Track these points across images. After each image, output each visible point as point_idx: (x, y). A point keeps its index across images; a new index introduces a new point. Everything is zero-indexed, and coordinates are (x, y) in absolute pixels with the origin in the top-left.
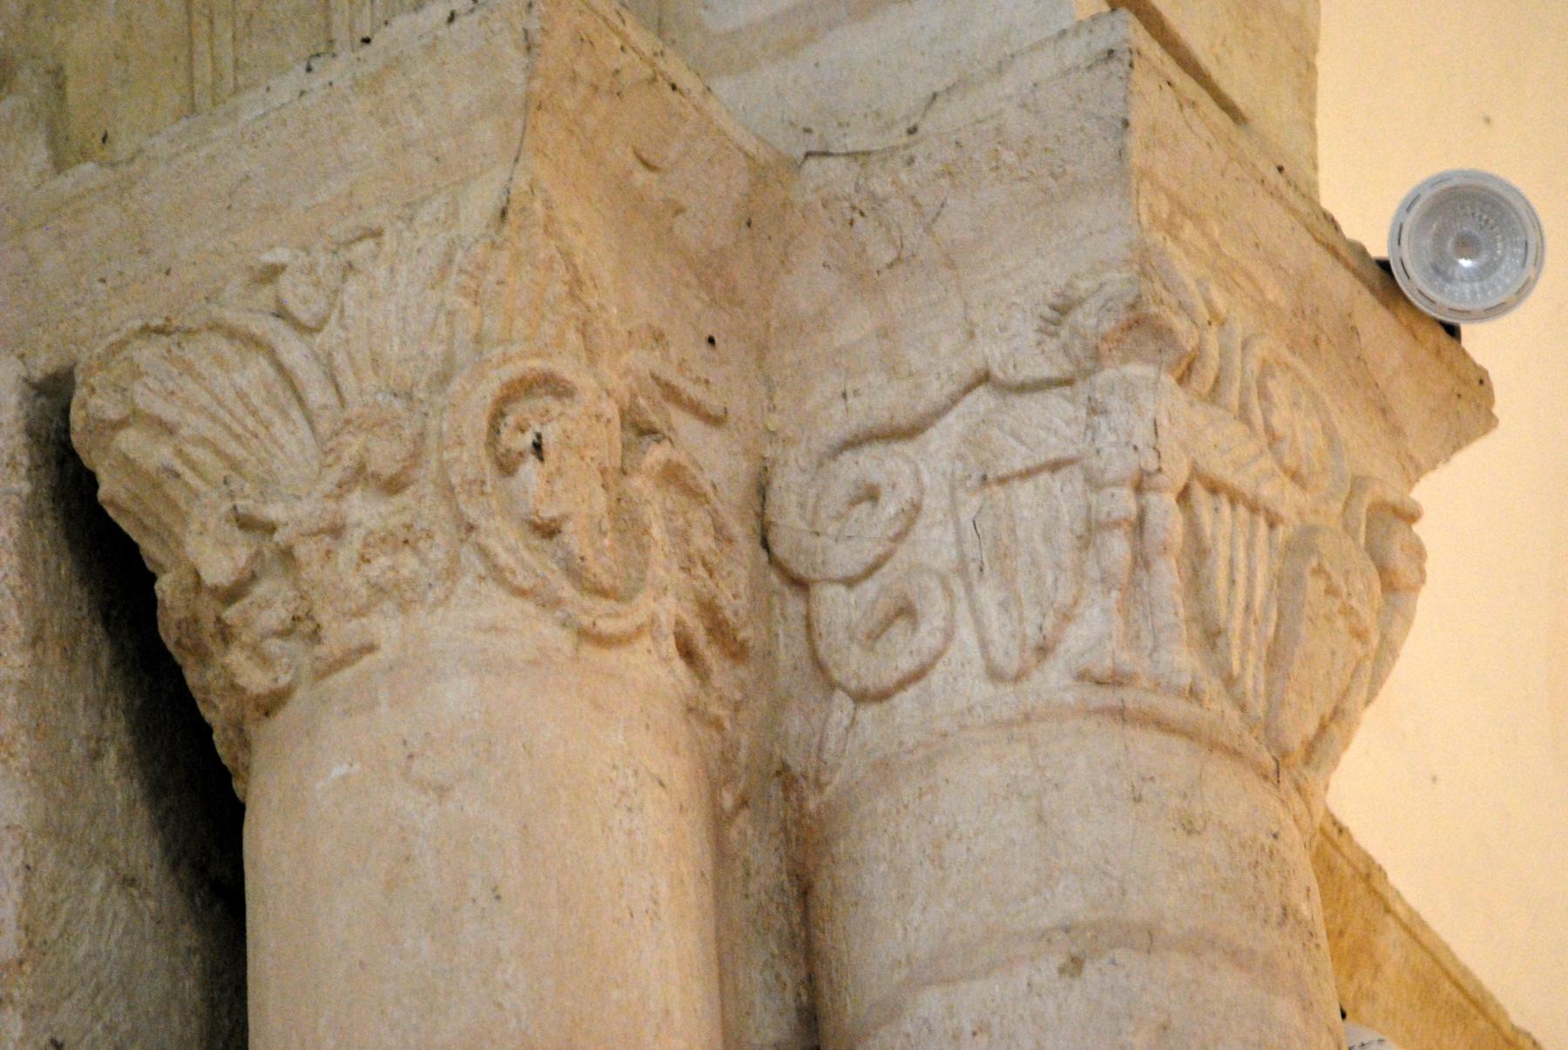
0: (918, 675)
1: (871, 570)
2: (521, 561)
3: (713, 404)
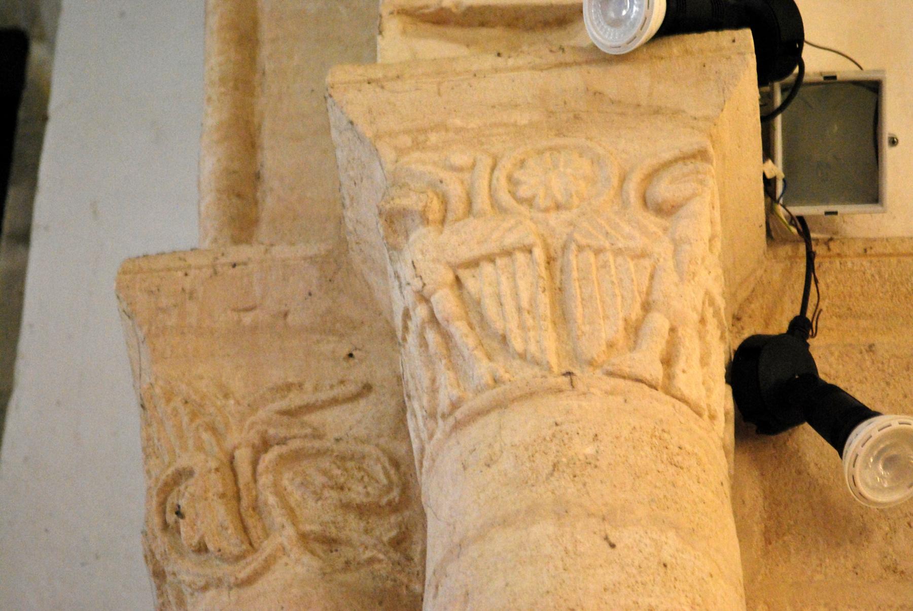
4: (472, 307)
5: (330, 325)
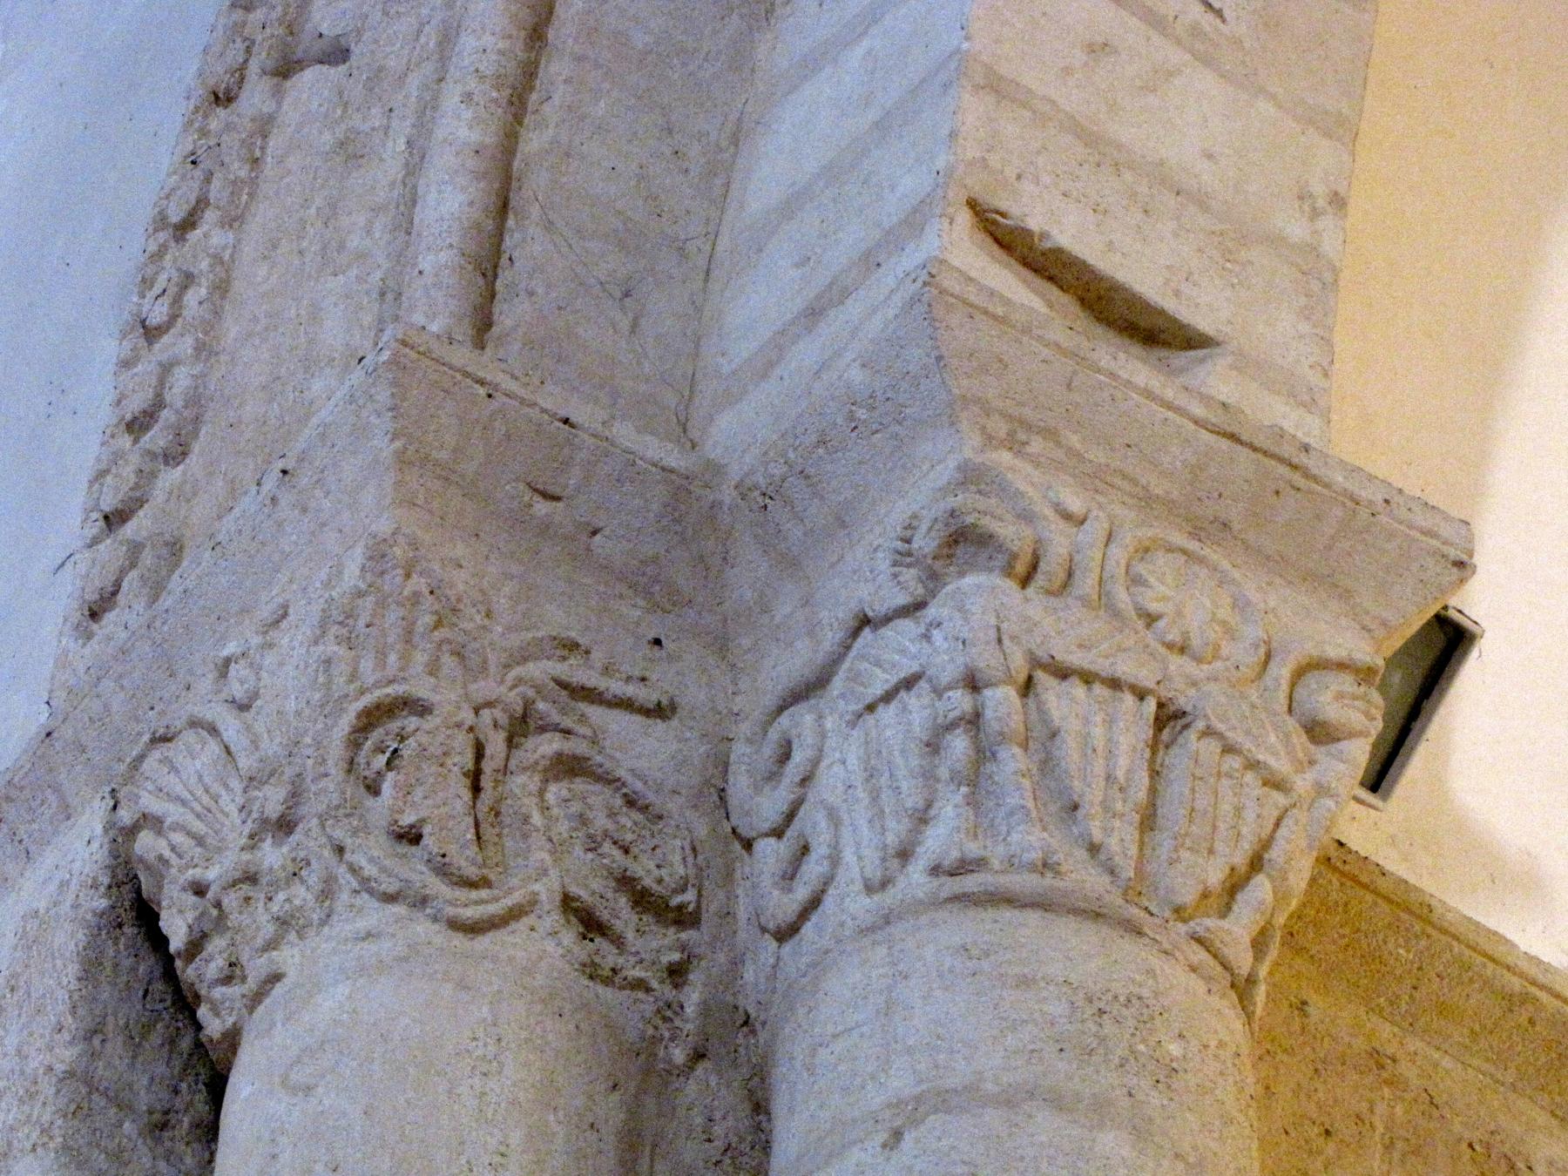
2: (383, 870)
4: (1043, 740)
5: (646, 583)
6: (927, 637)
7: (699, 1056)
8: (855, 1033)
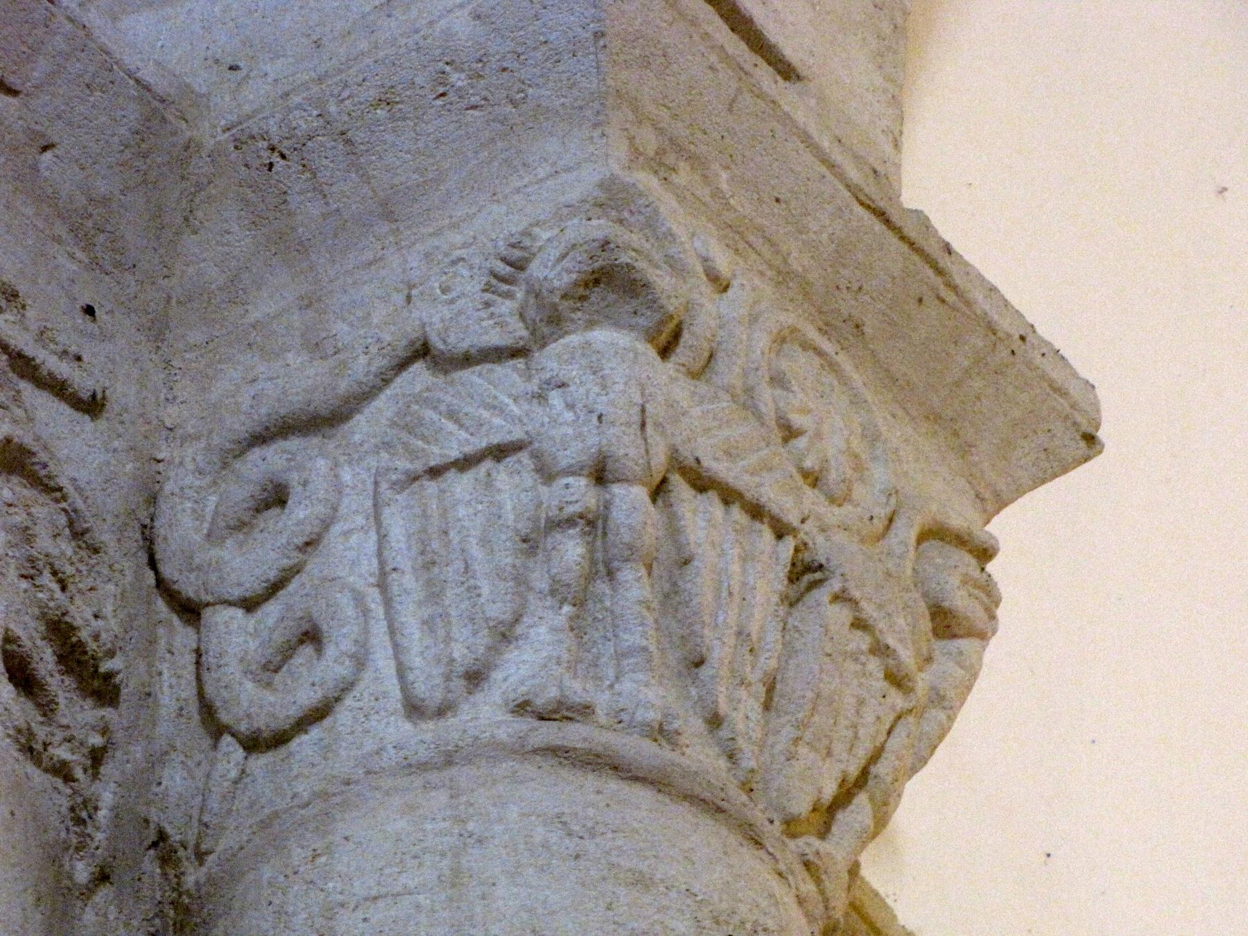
0: (319, 713)
1: (275, 588)
3: (82, 382)
5: (88, 228)
6: (541, 397)
7: (103, 877)
8: (406, 901)
